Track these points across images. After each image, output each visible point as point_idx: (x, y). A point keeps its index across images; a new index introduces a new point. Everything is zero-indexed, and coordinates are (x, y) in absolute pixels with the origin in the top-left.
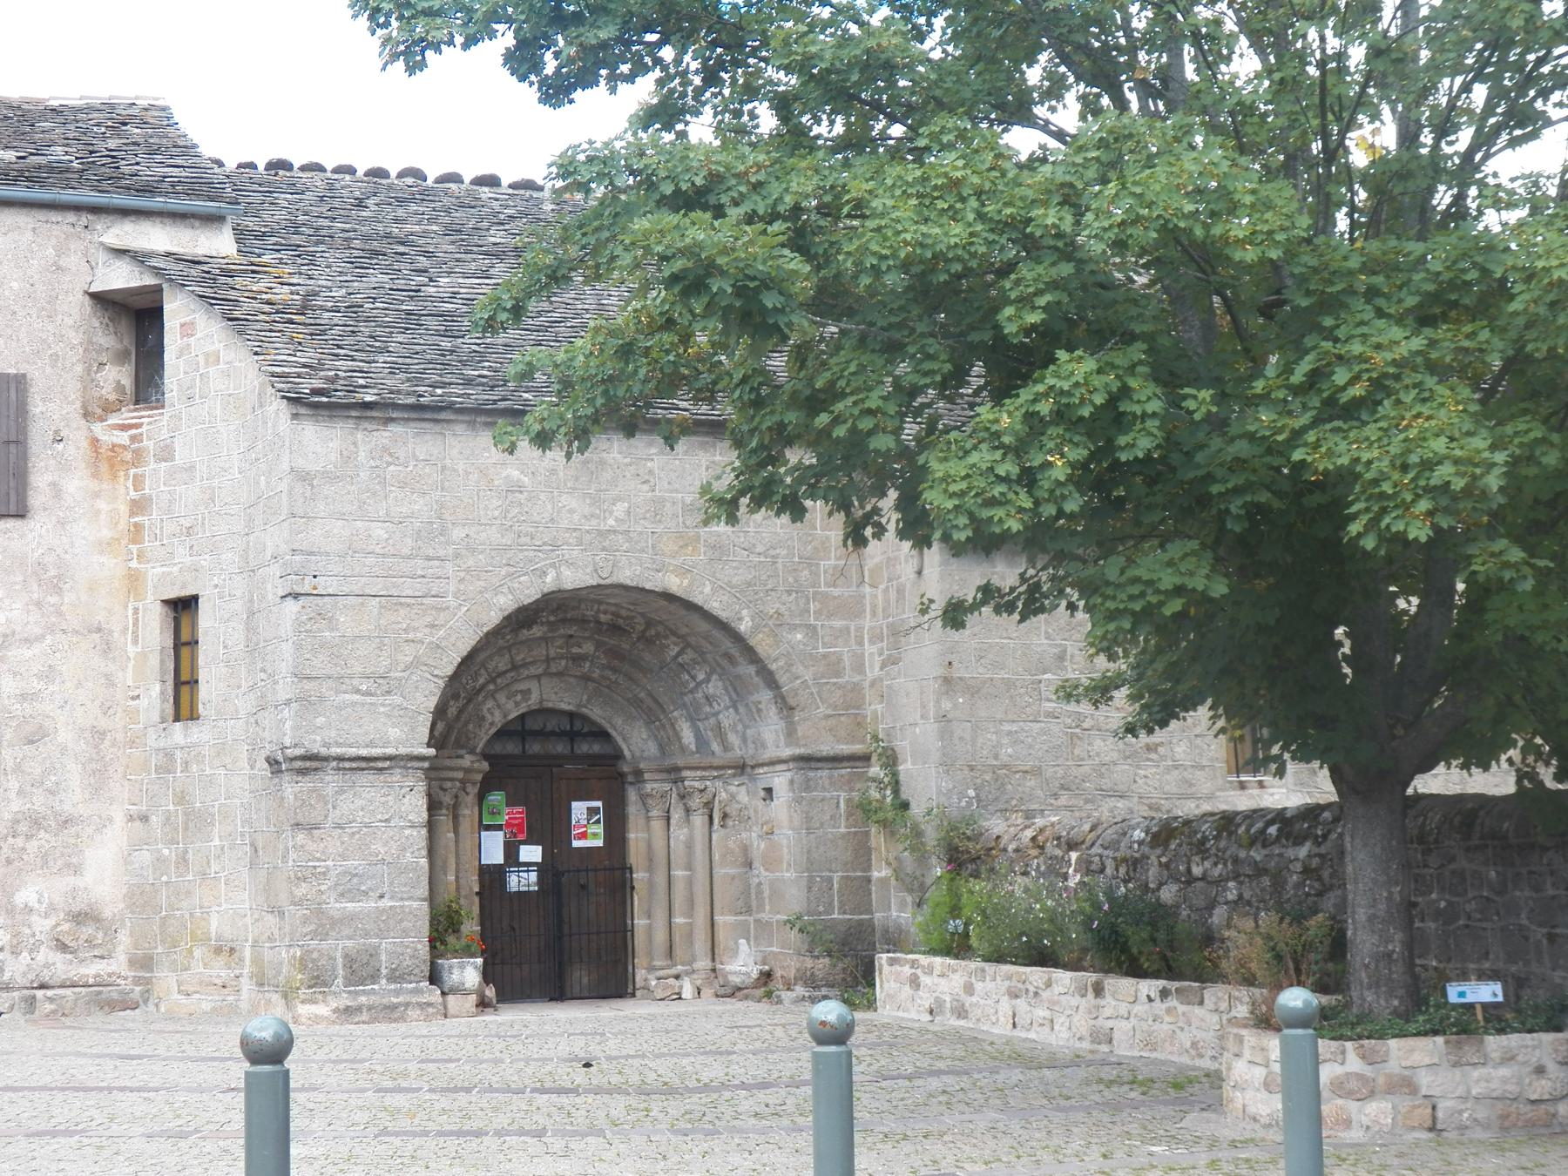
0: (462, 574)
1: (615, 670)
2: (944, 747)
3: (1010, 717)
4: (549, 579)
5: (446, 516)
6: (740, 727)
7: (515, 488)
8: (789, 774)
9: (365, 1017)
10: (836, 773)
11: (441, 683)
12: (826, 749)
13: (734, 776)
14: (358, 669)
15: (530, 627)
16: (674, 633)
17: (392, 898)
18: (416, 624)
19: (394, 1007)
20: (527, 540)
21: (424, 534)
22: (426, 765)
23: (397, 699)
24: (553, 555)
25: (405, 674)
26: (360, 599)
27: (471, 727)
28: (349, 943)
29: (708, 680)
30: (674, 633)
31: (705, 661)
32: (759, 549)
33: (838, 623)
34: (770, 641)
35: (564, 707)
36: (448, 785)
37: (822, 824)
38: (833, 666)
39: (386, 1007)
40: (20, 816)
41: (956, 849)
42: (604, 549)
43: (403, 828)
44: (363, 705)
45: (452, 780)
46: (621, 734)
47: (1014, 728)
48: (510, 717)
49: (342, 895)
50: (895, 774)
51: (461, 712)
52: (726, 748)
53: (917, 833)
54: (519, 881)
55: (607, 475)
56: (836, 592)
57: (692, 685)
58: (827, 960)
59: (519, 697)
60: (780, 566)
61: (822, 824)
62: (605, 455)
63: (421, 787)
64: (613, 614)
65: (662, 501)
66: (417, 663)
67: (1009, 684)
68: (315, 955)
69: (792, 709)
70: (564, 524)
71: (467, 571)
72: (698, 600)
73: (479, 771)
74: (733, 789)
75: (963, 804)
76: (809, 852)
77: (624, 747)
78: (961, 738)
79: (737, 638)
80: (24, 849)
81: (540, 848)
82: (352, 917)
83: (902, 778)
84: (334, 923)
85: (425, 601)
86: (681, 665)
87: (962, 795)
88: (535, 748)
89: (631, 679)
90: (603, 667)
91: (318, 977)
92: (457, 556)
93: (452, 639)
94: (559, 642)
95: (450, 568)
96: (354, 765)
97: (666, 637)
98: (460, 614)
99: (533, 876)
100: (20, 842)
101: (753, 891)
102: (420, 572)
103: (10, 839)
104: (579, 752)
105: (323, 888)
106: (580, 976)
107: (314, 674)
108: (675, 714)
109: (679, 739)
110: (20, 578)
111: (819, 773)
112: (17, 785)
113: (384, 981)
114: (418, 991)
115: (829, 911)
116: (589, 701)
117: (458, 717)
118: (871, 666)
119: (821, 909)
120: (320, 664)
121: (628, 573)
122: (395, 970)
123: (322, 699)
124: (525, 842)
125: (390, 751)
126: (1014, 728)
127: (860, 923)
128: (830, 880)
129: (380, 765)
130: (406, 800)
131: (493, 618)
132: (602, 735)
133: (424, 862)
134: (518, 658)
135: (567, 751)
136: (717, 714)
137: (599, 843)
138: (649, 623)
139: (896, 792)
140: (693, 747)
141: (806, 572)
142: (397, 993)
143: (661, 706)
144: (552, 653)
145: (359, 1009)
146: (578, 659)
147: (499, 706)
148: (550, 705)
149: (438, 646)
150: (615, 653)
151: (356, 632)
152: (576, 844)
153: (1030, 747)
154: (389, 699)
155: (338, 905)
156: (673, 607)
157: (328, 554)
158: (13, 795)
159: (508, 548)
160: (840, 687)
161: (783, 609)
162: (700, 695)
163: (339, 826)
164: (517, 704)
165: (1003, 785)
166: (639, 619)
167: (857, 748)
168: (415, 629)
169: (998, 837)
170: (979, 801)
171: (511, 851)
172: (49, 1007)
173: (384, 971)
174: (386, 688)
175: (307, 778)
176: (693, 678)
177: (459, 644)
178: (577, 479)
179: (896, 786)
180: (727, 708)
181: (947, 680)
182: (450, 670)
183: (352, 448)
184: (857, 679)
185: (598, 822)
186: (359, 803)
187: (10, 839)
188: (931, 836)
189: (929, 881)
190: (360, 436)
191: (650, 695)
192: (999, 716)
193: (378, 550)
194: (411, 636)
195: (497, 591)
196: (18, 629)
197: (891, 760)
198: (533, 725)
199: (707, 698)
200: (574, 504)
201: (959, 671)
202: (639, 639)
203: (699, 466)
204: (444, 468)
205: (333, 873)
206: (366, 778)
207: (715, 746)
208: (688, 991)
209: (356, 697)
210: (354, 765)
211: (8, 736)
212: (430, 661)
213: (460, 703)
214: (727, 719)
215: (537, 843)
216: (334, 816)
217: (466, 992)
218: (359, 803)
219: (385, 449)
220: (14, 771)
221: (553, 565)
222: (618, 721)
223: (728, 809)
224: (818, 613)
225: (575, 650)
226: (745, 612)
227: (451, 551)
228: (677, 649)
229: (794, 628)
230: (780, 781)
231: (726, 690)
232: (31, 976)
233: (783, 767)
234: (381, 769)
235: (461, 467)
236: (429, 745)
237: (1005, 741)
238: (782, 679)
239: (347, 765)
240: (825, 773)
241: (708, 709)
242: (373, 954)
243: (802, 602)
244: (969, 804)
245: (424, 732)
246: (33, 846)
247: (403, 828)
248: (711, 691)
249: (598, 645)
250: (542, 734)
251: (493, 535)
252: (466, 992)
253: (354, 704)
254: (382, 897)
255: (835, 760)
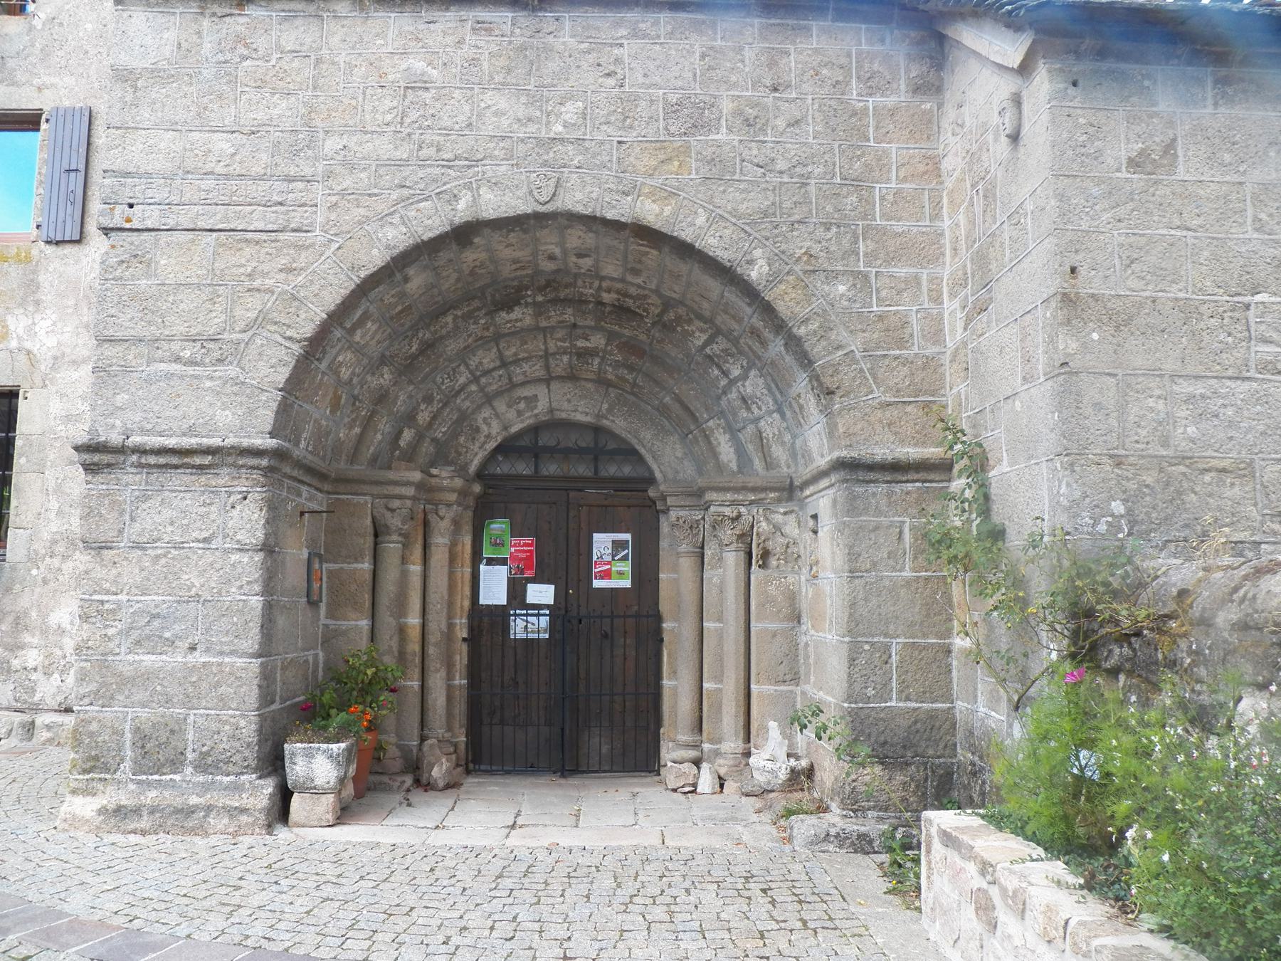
0: (334, 199)
1: (631, 368)
2: (1064, 421)
3: (1190, 370)
4: (462, 205)
5: (318, 123)
6: (787, 438)
7: (418, 85)
8: (831, 492)
9: (145, 823)
10: (897, 488)
11: (297, 349)
12: (882, 451)
13: (779, 500)
14: (180, 329)
15: (510, 309)
16: (700, 317)
17: (207, 650)
18: (266, 268)
19: (189, 811)
20: (432, 152)
21: (283, 146)
22: (264, 462)
23: (232, 371)
24: (471, 172)
25: (246, 336)
26: (190, 235)
27: (462, 439)
28: (143, 713)
29: (744, 377)
30: (700, 317)
31: (741, 353)
32: (781, 165)
33: (902, 271)
34: (796, 294)
35: (580, 417)
36: (396, 503)
37: (874, 564)
38: (896, 332)
39: (177, 811)
40: (58, 537)
41: (1089, 614)
42: (545, 164)
43: (227, 551)
44: (182, 377)
45: (401, 497)
46: (650, 450)
47: (1199, 389)
48: (514, 429)
49: (138, 643)
50: (984, 486)
51: (434, 418)
52: (769, 464)
53: (1019, 582)
54: (524, 627)
55: (553, 65)
56: (898, 227)
57: (724, 382)
58: (878, 769)
59: (522, 405)
60: (812, 189)
61: (874, 564)
62: (551, 39)
63: (257, 494)
64: (618, 292)
65: (633, 99)
66: (261, 321)
67: (1188, 311)
68: (94, 727)
69: (831, 393)
70: (489, 130)
71: (343, 194)
72: (687, 235)
73: (453, 490)
74: (778, 518)
75: (1102, 528)
76: (853, 605)
77: (654, 467)
78: (1098, 406)
79: (749, 291)
80: (59, 570)
81: (552, 588)
82: (145, 678)
83: (994, 491)
84: (125, 682)
85: (281, 236)
86: (709, 357)
87: (1099, 511)
88: (551, 468)
89: (657, 382)
90: (617, 365)
91: (96, 758)
92: (329, 175)
93: (315, 288)
94: (560, 334)
95: (318, 190)
96: (162, 460)
97: (690, 322)
98: (329, 253)
99: (544, 621)
100: (56, 562)
101: (801, 652)
102: (276, 198)
103: (47, 559)
104: (603, 474)
105: (111, 632)
106: (598, 743)
107: (119, 334)
108: (711, 423)
109: (715, 455)
110: (72, 302)
111: (872, 488)
112: (57, 506)
113: (189, 770)
114: (236, 788)
115: (884, 695)
116: (610, 410)
117: (430, 425)
118: (953, 330)
119: (870, 692)
120: (128, 323)
121: (579, 196)
122: (208, 754)
123: (127, 369)
124: (534, 580)
125: (215, 442)
126: (1199, 389)
127: (933, 715)
128: (887, 648)
129: (198, 460)
130: (235, 513)
131: (376, 258)
132: (630, 453)
133: (256, 602)
134: (509, 353)
135: (590, 474)
136: (756, 420)
137: (626, 583)
138: (667, 304)
139: (985, 512)
140: (734, 466)
141: (854, 199)
142: (206, 787)
143: (692, 415)
144: (552, 347)
145: (137, 811)
146: (584, 354)
147: (497, 416)
148: (564, 415)
149: (294, 298)
150: (631, 347)
151: (181, 278)
152: (597, 584)
153: (1231, 424)
154: (221, 371)
155: (130, 657)
156: (683, 267)
157: (149, 175)
158: (52, 515)
159: (401, 164)
160: (906, 362)
161: (816, 249)
162: (733, 395)
163: (137, 546)
164: (519, 413)
165: (1179, 493)
166: (654, 299)
167: (932, 452)
168: (264, 275)
169: (1183, 593)
170: (1132, 523)
171: (516, 590)
172: (46, 735)
173: (190, 756)
174: (217, 355)
175: (99, 478)
176: (725, 373)
177: (325, 294)
178: (509, 71)
179: (985, 502)
180: (770, 413)
181: (1068, 300)
182: (308, 330)
183: (195, 37)
184: (931, 350)
185: (625, 558)
186: (168, 513)
187: (47, 559)
188: (1040, 587)
189: (1036, 668)
190: (206, 23)
191: (678, 399)
192: (1169, 366)
193: (220, 169)
194: (257, 283)
195: (383, 219)
196: (68, 351)
197: (979, 465)
198: (546, 439)
199: (744, 400)
200: (503, 104)
201: (1089, 284)
202: (654, 324)
203: (692, 53)
204: (318, 61)
205: (125, 613)
206: (179, 479)
207: (758, 464)
208: (706, 781)
209: (176, 368)
210: (162, 460)
211: (52, 457)
212: (282, 318)
213: (436, 406)
214: (771, 425)
215: (548, 582)
216: (133, 531)
217: (318, 792)
218: (168, 513)
219: (239, 39)
220: (55, 492)
221: (468, 186)
222: (647, 435)
223: (770, 545)
224: (871, 257)
225: (581, 343)
226: (758, 253)
227: (320, 169)
228: (704, 337)
229: (832, 276)
230: (824, 501)
231: (770, 390)
232: (60, 698)
233: (824, 483)
234: (201, 467)
235: (341, 60)
236: (272, 435)
237: (1182, 413)
238: (816, 349)
239: (152, 460)
240: (882, 488)
241: (744, 414)
242: (175, 730)
243: (846, 242)
244: (1114, 527)
245: (267, 417)
246: (68, 567)
247: (227, 551)
248: (749, 390)
249: (611, 336)
250: (566, 453)
251: (383, 147)
252: (318, 792)
253: (169, 376)
254: (193, 648)
255: (897, 468)
